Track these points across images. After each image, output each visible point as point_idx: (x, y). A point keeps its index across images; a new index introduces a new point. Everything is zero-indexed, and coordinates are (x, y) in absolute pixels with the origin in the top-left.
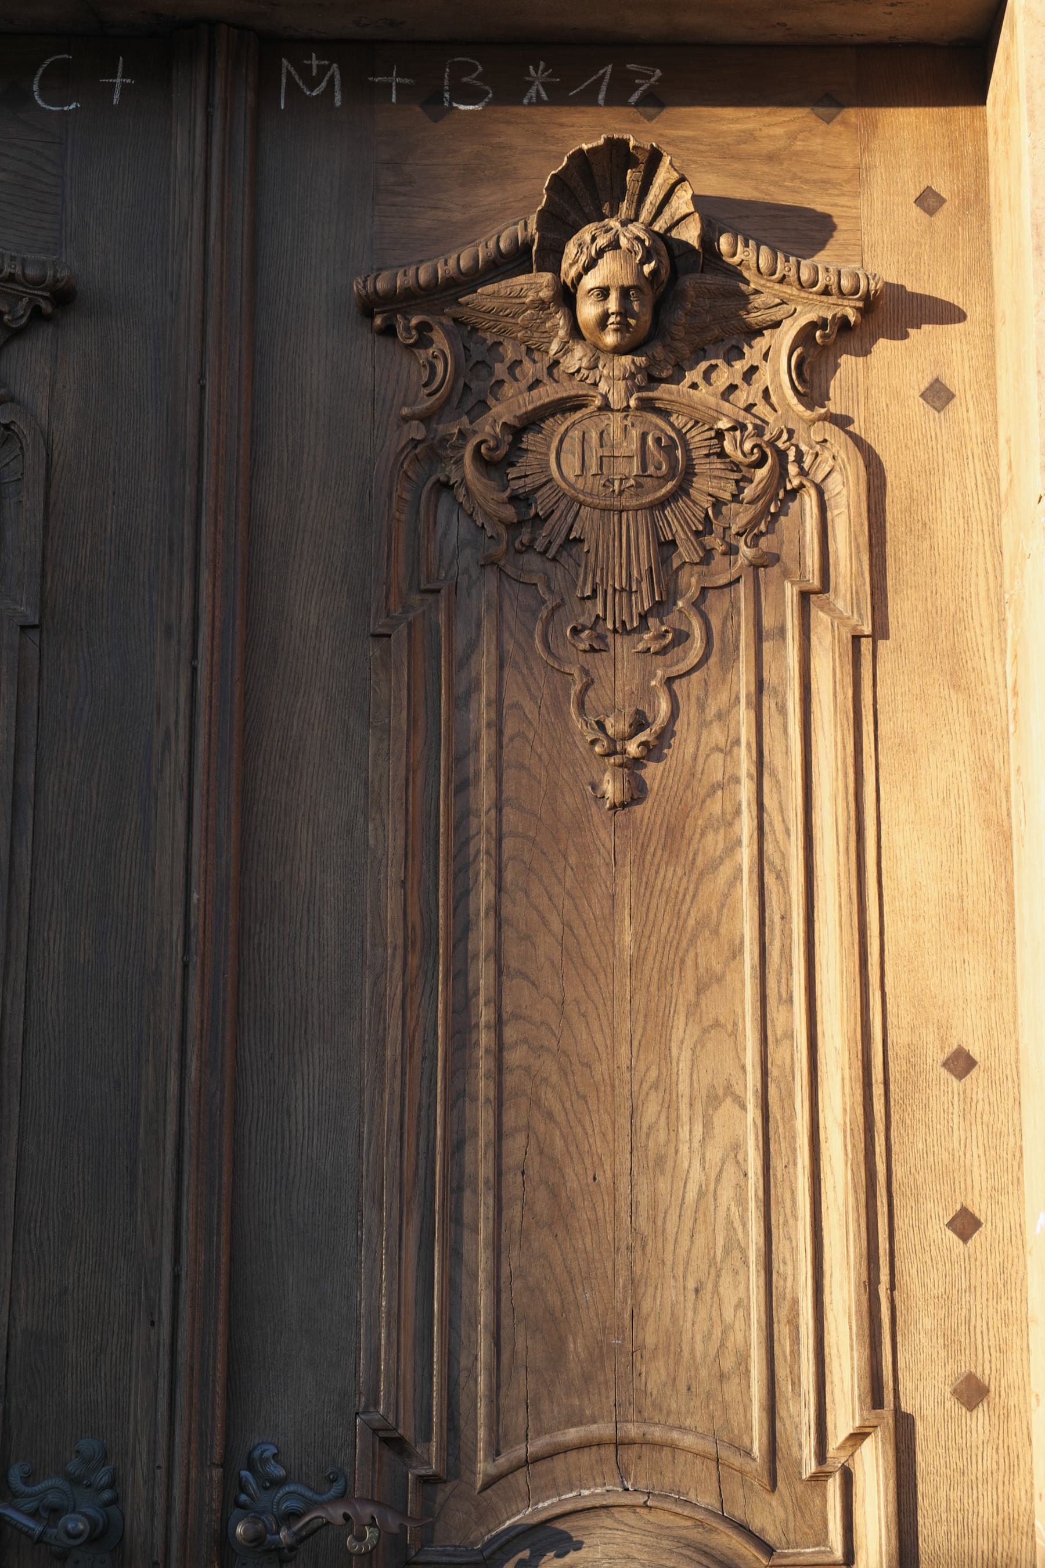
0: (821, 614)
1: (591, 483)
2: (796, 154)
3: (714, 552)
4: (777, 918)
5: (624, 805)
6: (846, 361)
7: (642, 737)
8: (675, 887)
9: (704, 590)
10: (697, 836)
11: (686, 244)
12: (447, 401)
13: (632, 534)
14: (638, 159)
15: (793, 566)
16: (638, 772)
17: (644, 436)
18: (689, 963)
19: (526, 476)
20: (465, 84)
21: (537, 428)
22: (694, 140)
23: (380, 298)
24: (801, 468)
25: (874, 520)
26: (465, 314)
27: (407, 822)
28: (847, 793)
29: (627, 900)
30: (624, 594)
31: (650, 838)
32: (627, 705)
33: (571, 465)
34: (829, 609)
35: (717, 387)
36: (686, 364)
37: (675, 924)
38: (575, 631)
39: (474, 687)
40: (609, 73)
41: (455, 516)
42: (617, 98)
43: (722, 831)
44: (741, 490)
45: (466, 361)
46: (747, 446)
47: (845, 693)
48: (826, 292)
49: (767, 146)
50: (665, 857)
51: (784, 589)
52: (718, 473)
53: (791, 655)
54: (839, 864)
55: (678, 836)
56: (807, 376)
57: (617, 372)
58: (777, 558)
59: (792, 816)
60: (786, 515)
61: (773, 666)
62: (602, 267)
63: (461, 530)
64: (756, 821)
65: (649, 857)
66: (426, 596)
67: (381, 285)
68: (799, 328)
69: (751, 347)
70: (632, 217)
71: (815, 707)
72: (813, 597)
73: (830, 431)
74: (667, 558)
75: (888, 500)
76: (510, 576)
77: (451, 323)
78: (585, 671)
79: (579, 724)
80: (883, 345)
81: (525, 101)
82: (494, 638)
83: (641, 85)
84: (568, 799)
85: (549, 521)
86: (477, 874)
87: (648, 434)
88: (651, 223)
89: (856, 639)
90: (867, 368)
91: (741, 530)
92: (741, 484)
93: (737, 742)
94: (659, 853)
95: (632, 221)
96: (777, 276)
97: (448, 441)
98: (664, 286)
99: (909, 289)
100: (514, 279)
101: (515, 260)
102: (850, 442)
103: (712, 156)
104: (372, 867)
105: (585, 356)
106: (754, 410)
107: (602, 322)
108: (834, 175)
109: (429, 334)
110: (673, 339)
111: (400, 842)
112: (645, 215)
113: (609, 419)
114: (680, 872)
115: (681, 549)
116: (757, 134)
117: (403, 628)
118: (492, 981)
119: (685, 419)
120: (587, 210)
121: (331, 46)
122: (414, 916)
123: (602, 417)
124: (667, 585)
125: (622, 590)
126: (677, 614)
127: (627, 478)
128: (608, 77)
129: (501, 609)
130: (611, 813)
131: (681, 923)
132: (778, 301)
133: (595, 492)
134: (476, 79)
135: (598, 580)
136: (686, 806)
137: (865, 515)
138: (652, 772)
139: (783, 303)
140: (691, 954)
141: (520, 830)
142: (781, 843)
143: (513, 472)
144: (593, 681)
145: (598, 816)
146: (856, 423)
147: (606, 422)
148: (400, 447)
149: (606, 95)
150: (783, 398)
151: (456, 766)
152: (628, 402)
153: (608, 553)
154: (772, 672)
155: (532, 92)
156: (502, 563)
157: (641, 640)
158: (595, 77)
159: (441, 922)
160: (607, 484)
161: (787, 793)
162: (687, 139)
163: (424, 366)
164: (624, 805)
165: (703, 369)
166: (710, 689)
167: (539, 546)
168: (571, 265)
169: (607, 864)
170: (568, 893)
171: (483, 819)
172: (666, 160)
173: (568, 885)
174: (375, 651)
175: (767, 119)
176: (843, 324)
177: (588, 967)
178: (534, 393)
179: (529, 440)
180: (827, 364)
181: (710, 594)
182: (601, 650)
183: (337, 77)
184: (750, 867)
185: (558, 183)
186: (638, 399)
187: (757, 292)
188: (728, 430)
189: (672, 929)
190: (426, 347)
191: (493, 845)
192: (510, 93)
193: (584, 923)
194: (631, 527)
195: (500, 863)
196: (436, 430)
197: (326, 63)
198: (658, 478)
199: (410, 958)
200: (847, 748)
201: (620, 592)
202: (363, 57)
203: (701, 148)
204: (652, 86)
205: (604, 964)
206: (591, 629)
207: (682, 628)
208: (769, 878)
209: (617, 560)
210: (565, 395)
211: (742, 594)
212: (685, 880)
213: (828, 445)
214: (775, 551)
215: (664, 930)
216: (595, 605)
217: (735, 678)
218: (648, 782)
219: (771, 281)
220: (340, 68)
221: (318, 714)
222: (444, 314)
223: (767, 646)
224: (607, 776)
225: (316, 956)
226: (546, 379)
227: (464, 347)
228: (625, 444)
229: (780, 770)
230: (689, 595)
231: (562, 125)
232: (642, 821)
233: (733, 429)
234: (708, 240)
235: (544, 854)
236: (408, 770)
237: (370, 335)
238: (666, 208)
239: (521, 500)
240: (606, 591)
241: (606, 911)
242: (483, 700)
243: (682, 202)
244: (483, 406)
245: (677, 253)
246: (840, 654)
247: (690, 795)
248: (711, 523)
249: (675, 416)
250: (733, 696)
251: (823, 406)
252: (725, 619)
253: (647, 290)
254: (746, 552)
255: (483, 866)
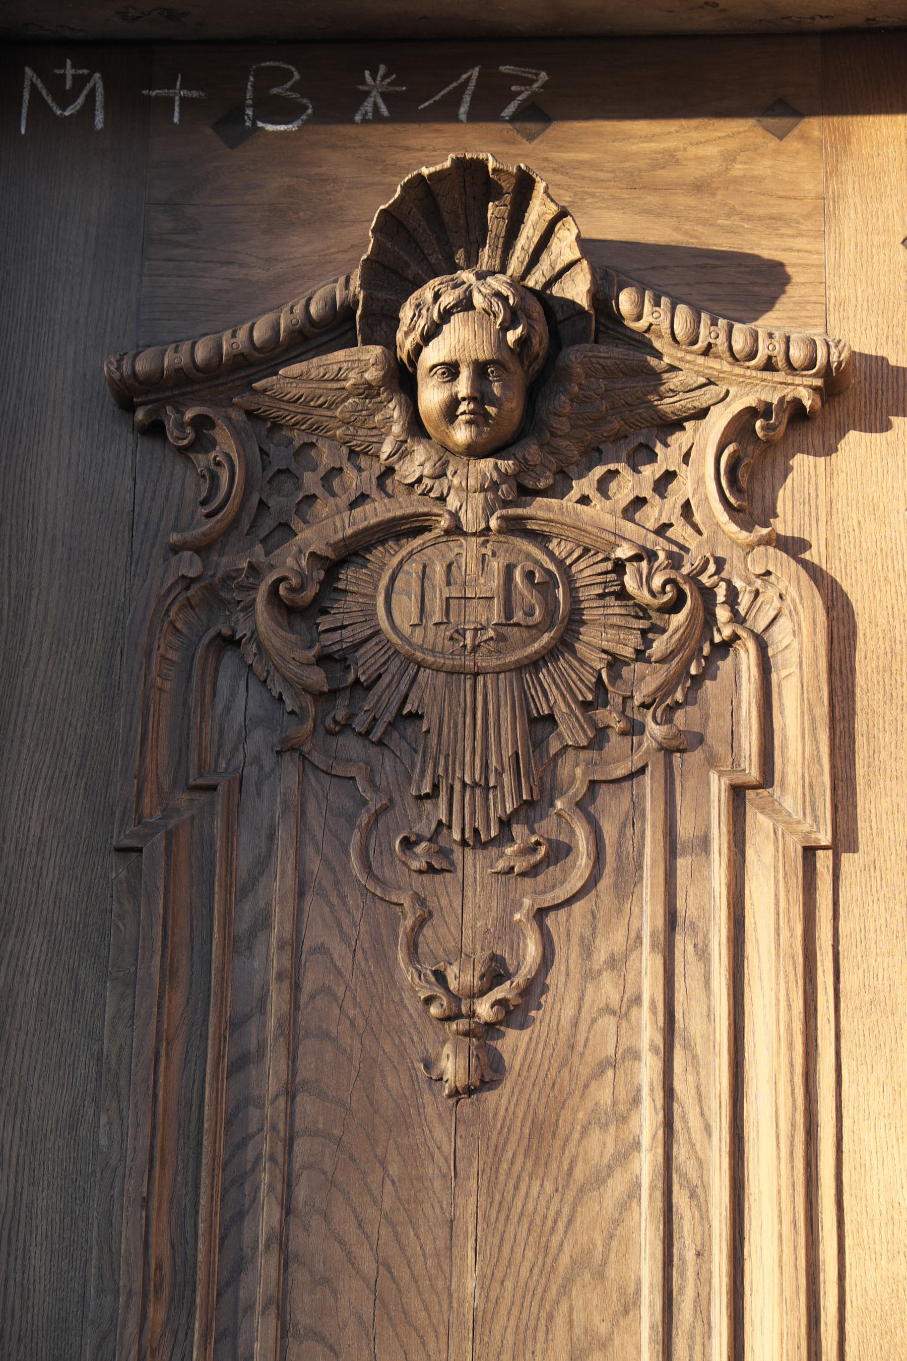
0: (761, 817)
1: (429, 638)
2: (735, 181)
3: (609, 731)
4: (690, 1255)
5: (470, 1091)
6: (802, 463)
7: (499, 993)
8: (541, 1209)
9: (593, 784)
10: (576, 1136)
11: (571, 304)
12: (234, 523)
13: (490, 707)
14: (501, 187)
15: (722, 749)
16: (492, 1043)
17: (509, 570)
18: (560, 1320)
19: (343, 627)
20: (277, 97)
21: (360, 561)
22: (591, 165)
23: (141, 383)
24: (735, 613)
25: (838, 684)
26: (262, 404)
27: (154, 1114)
28: (792, 1073)
29: (471, 1228)
30: (478, 791)
31: (507, 1140)
32: (478, 947)
33: (406, 609)
34: (773, 809)
35: (617, 501)
36: (573, 470)
37: (540, 1262)
38: (408, 844)
39: (263, 922)
40: (474, 78)
41: (243, 684)
42: (486, 110)
43: (612, 1129)
44: (648, 644)
45: (264, 469)
46: (657, 582)
47: (791, 930)
48: (769, 366)
49: (693, 171)
50: (529, 1165)
51: (708, 783)
52: (617, 621)
53: (717, 875)
54: (779, 1176)
55: (549, 1136)
56: (744, 483)
57: (471, 481)
58: (700, 739)
59: (715, 1105)
60: (714, 678)
61: (691, 892)
62: (453, 335)
63: (251, 703)
64: (661, 1114)
65: (505, 1166)
66: (196, 795)
67: (142, 366)
68: (730, 416)
69: (667, 445)
70: (497, 268)
71: (750, 949)
72: (750, 794)
73: (776, 560)
74: (542, 741)
75: (859, 655)
76: (317, 767)
77: (243, 417)
78: (420, 900)
79: (407, 974)
80: (855, 441)
81: (358, 118)
82: (292, 853)
83: (519, 93)
84: (391, 1082)
85: (374, 690)
86: (256, 1190)
87: (515, 566)
88: (524, 277)
89: (810, 852)
90: (831, 474)
91: (648, 700)
92: (650, 636)
93: (637, 1000)
94: (520, 1159)
95: (493, 273)
96: (701, 344)
97: (234, 579)
98: (540, 361)
99: (893, 362)
100: (330, 356)
101: (334, 329)
102: (803, 573)
103: (607, 185)
104: (102, 1178)
105: (428, 459)
106: (669, 533)
107: (450, 411)
108: (789, 208)
109: (211, 432)
110: (553, 435)
111: (144, 1143)
112: (515, 265)
113: (461, 546)
114: (549, 1187)
115: (562, 727)
116: (680, 155)
117: (159, 839)
118: (271, 1342)
119: (570, 546)
120: (433, 260)
121: (91, 49)
122: (161, 1248)
123: (451, 544)
124: (541, 778)
125: (475, 784)
126: (554, 817)
127: (484, 628)
128: (473, 83)
129: (303, 813)
130: (451, 1102)
131: (549, 1261)
132: (703, 380)
133: (439, 648)
134: (290, 90)
135: (441, 772)
136: (560, 1092)
137: (824, 676)
138: (513, 1044)
139: (710, 383)
140: (564, 1306)
141: (321, 1126)
142: (698, 1147)
143: (325, 622)
144: (430, 914)
145: (433, 1106)
146: (814, 549)
147: (457, 550)
148: (166, 587)
149: (471, 107)
150: (711, 515)
151: (231, 1035)
152: (488, 522)
153: (456, 733)
154: (691, 900)
155: (368, 106)
156: (306, 749)
157: (502, 855)
158: (455, 84)
159: (200, 1257)
160: (456, 636)
161: (708, 1073)
162: (581, 164)
163: (203, 476)
164: (470, 1091)
165: (597, 477)
166: (600, 925)
167: (360, 724)
168: (407, 334)
169: (444, 1176)
170: (386, 1218)
171: (268, 1110)
172: (540, 186)
173: (386, 1206)
174: (119, 872)
175: (695, 135)
176: (797, 414)
177: (412, 1326)
178: (358, 512)
179: (349, 576)
180: (773, 467)
181: (603, 789)
182: (443, 871)
183: (100, 90)
184: (652, 1181)
185: (391, 223)
186: (501, 518)
187: (672, 368)
188: (631, 559)
189: (536, 1271)
190: (207, 451)
191: (280, 1147)
192: (337, 105)
193: (409, 1262)
194: (490, 697)
195: (290, 1174)
196: (218, 564)
197: (86, 72)
198: (528, 627)
199: (151, 1310)
200: (794, 1007)
201: (472, 788)
202: (134, 62)
203: (602, 175)
204: (534, 94)
205: (435, 1321)
206: (430, 840)
207: (562, 838)
208: (680, 1198)
209: (468, 743)
210: (398, 513)
211: (648, 790)
212: (557, 1197)
213: (772, 579)
214: (697, 729)
215: (524, 1272)
216: (436, 806)
217: (636, 910)
218: (506, 1057)
219: (691, 352)
220: (104, 79)
221: (35, 959)
222: (233, 405)
223: (682, 863)
224: (447, 1049)
225: (17, 1308)
226: (375, 493)
227: (261, 449)
228: (482, 581)
229: (698, 1040)
230: (572, 792)
231: (407, 149)
232: (496, 1114)
233: (637, 558)
234: (603, 298)
235: (354, 1160)
236: (158, 1040)
237: (130, 436)
238: (544, 256)
239: (336, 660)
240: (452, 787)
241: (441, 1244)
242: (274, 941)
243: (564, 247)
244: (286, 530)
245: (560, 316)
246: (786, 874)
247: (567, 1077)
248: (606, 690)
249: (555, 541)
250: (633, 935)
251: (766, 525)
252: (623, 825)
253: (514, 366)
254: (655, 730)
255: (265, 1178)
